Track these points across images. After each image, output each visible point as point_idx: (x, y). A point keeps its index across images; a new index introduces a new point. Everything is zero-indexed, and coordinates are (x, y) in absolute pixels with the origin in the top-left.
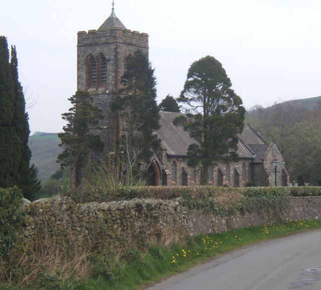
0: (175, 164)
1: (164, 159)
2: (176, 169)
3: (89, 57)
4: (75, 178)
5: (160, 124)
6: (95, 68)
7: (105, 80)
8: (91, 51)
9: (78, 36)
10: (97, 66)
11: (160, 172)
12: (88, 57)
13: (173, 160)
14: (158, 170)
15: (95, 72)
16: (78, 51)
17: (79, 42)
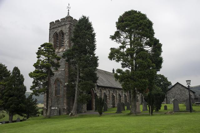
0: (101, 91)
1: (96, 88)
2: (101, 94)
3: (55, 34)
4: (46, 99)
5: (169, 81)
6: (58, 41)
7: (63, 43)
8: (56, 31)
9: (50, 25)
10: (59, 39)
11: (94, 95)
12: (54, 34)
13: (100, 88)
14: (93, 94)
15: (58, 41)
16: (50, 31)
17: (50, 27)
